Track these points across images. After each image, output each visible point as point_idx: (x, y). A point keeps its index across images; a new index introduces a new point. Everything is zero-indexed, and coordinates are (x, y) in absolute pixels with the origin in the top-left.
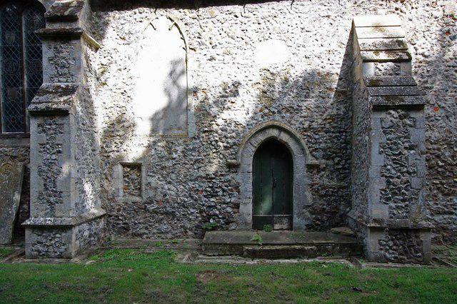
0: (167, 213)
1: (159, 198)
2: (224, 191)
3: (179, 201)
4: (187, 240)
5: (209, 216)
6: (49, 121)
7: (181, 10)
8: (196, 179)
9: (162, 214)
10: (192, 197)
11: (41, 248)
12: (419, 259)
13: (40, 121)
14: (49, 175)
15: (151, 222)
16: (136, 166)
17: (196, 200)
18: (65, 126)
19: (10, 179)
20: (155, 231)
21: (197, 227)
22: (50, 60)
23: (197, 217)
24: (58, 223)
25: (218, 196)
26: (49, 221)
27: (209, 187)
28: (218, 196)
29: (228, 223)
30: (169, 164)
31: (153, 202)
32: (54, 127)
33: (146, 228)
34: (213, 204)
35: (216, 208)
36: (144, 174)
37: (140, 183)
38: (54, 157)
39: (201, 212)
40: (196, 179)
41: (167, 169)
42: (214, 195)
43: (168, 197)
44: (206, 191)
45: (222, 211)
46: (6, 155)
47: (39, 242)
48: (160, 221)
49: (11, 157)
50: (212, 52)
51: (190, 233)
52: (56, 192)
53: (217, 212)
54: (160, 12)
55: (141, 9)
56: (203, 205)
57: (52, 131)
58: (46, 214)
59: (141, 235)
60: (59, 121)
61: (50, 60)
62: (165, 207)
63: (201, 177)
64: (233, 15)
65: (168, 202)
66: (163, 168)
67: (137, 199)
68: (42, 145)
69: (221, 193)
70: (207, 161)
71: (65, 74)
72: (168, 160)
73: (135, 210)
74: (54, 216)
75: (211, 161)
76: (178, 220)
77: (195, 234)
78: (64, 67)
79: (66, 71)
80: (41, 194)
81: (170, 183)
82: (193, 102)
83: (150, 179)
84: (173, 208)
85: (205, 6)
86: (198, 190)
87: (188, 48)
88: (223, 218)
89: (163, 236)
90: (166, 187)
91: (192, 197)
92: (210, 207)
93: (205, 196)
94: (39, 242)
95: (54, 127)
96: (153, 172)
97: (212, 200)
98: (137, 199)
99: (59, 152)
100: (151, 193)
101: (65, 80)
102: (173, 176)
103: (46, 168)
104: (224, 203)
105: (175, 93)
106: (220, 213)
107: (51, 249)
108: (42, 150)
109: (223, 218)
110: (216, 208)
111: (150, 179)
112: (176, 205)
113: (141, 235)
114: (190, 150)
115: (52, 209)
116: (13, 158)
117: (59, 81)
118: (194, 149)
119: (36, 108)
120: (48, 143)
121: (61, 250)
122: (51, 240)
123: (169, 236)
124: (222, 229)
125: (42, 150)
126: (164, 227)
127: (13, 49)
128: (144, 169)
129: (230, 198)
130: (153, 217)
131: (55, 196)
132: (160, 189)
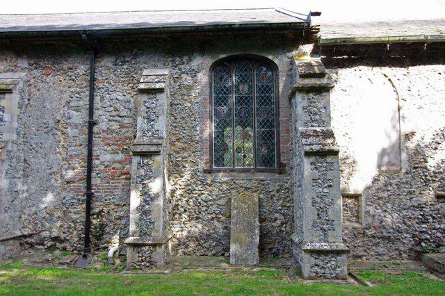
0: (383, 238)
1: (377, 224)
2: (434, 218)
3: (394, 227)
4: (402, 261)
5: (421, 240)
6: (320, 160)
7: (393, 68)
8: (409, 208)
9: (379, 238)
10: (405, 224)
11: (319, 270)
12: (29, 240)
13: (313, 159)
14: (322, 206)
15: (369, 245)
16: (356, 197)
17: (409, 226)
18: (335, 164)
19: (249, 207)
20: (373, 253)
21: (410, 250)
22: (304, 108)
23: (410, 241)
24: (335, 248)
25: (428, 222)
26: (326, 247)
27: (421, 215)
28: (428, 222)
29: (438, 246)
30: (385, 195)
31: (370, 228)
32: (325, 165)
33: (365, 251)
34: (424, 230)
35: (427, 233)
36: (363, 204)
37: (358, 212)
38: (326, 190)
39: (413, 236)
40: (409, 208)
41: (383, 199)
42: (425, 221)
43: (384, 223)
44: (418, 219)
45: (433, 236)
46: (241, 187)
47: (316, 265)
48: (377, 245)
49: (246, 188)
50: (421, 103)
51: (404, 255)
52: (328, 220)
53: (429, 237)
54: (377, 69)
55: (361, 67)
56: (416, 231)
57: (323, 169)
58: (320, 240)
59: (360, 257)
60: (329, 159)
61: (304, 108)
62: (382, 232)
63: (414, 206)
64: (437, 72)
65: (384, 228)
66: (379, 198)
67: (357, 225)
68: (314, 180)
69: (431, 220)
70: (418, 192)
71: (317, 120)
72: (383, 191)
73: (354, 235)
74: (328, 242)
75: (422, 192)
76: (393, 243)
77: (409, 256)
78: (316, 114)
79: (318, 117)
80: (315, 223)
81: (385, 211)
82: (411, 144)
83: (369, 208)
84: (390, 233)
85: (414, 65)
86: (410, 218)
87: (400, 99)
88: (434, 242)
89: (380, 258)
90: (382, 215)
91: (405, 224)
92: (421, 232)
93: (417, 223)
94: (316, 265)
95: (325, 165)
96: (371, 202)
97: (423, 226)
98: (357, 225)
99: (330, 186)
100: (370, 220)
101: (317, 125)
102: (389, 205)
103: (319, 200)
104: (434, 229)
105: (394, 137)
106: (431, 238)
107: (327, 271)
108: (315, 184)
109: (434, 242)
110: (427, 233)
111: (369, 208)
112: (391, 230)
113: (360, 257)
114: (403, 183)
115: (325, 235)
116: (247, 189)
117: (312, 126)
118: (407, 182)
119: (311, 149)
120: (319, 179)
121: (337, 272)
122: (327, 263)
123: (386, 257)
124: (434, 251)
125: (315, 184)
126: (381, 250)
127: (246, 98)
128: (363, 198)
129: (439, 224)
130: (371, 241)
131: (327, 224)
132: (377, 217)
